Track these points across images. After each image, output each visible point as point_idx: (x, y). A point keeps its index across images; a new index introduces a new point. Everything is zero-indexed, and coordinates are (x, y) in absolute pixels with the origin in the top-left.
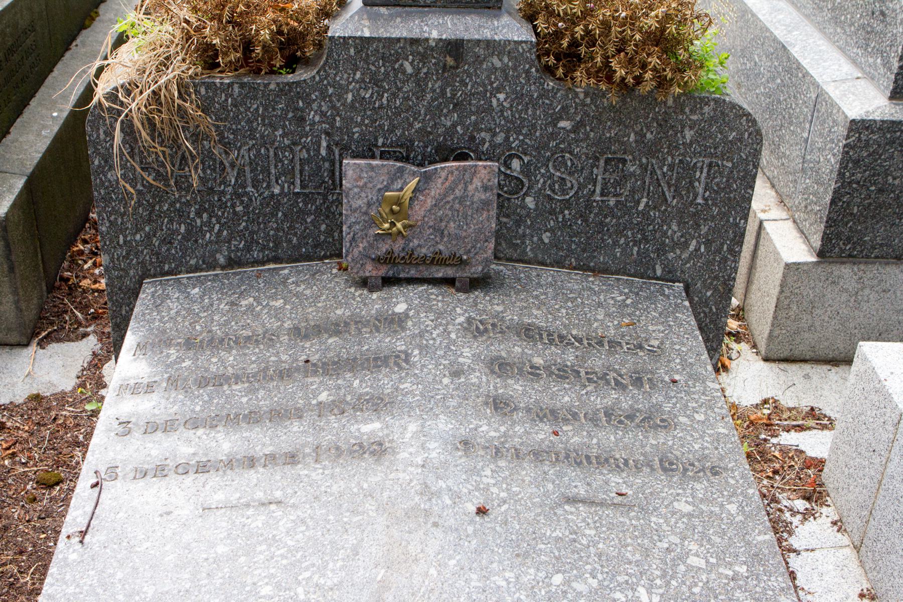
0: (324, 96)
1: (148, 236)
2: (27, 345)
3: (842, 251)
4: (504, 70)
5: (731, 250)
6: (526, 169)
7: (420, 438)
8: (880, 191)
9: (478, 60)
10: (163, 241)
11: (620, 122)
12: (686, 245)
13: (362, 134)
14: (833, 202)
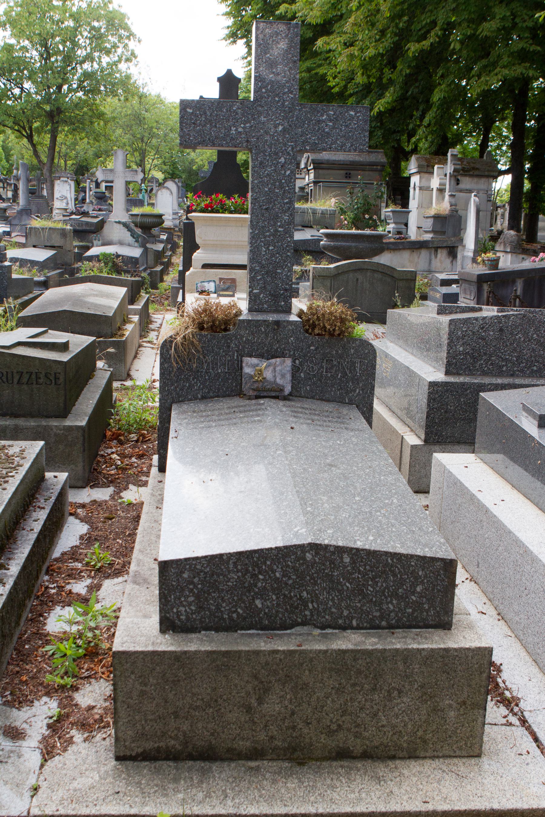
0: (236, 338)
1: (176, 388)
2: (85, 488)
3: (434, 440)
4: (293, 330)
5: (370, 393)
6: (300, 363)
7: (269, 420)
8: (446, 412)
9: (285, 327)
10: (180, 390)
11: (330, 347)
12: (355, 391)
13: (248, 351)
14: (427, 417)
